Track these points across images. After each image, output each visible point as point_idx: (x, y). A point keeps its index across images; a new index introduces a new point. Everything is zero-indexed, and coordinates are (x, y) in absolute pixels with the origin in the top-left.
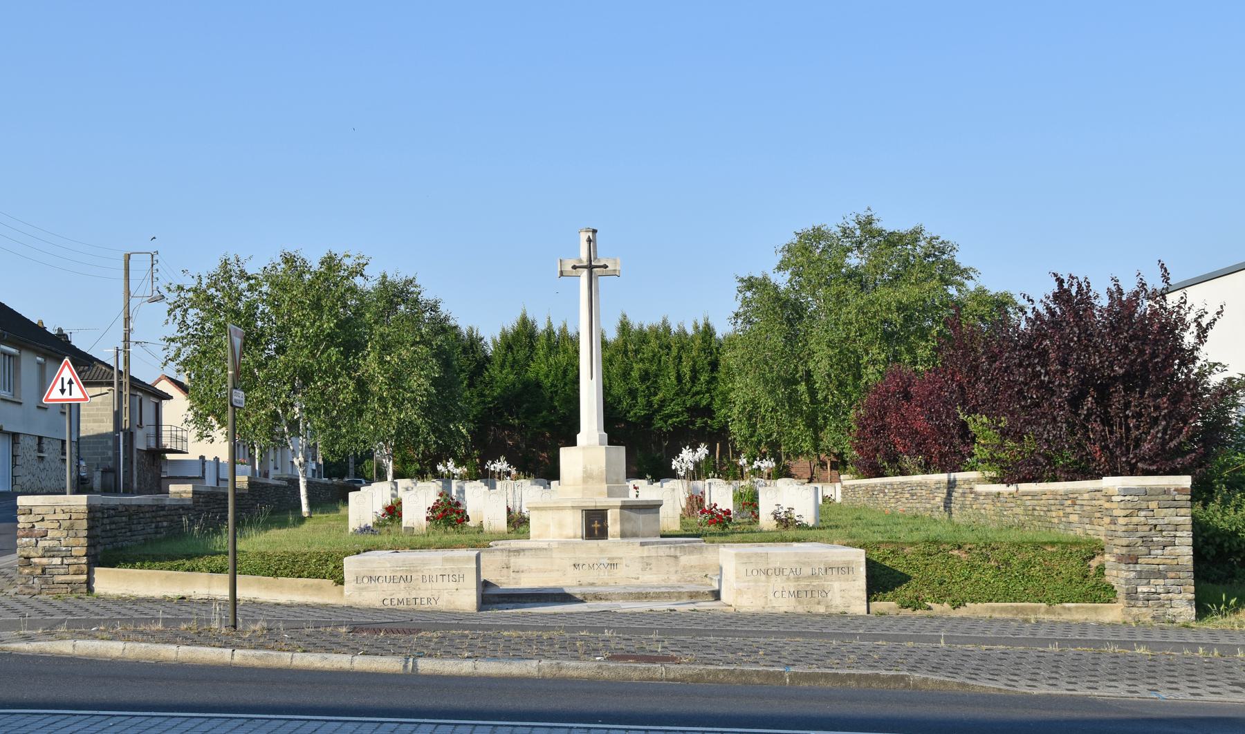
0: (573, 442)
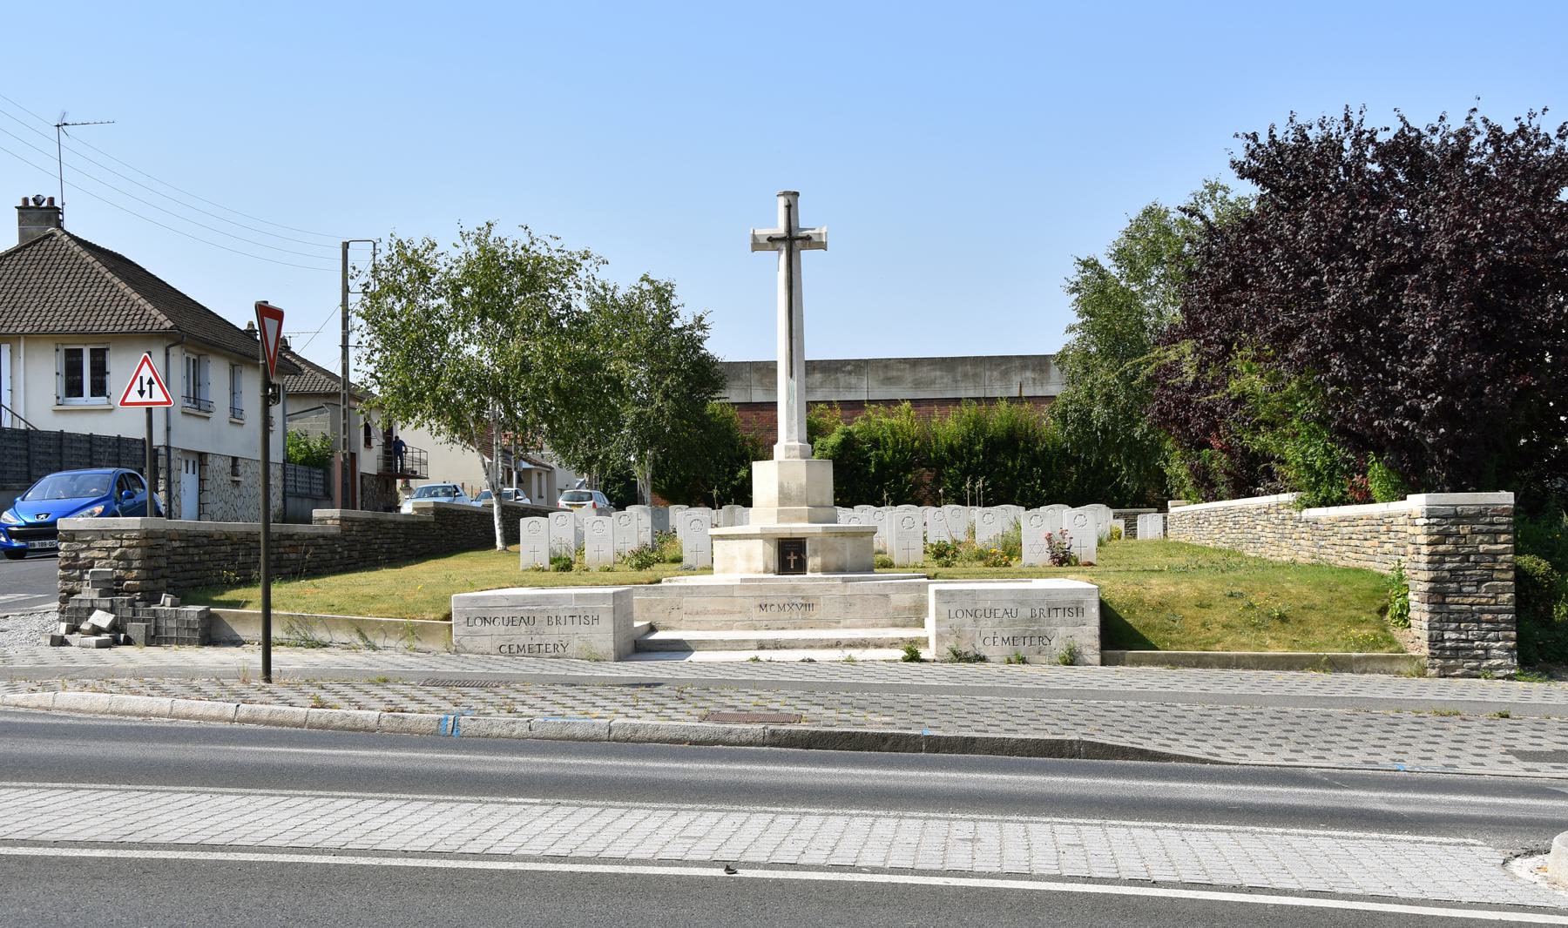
0: (768, 456)
